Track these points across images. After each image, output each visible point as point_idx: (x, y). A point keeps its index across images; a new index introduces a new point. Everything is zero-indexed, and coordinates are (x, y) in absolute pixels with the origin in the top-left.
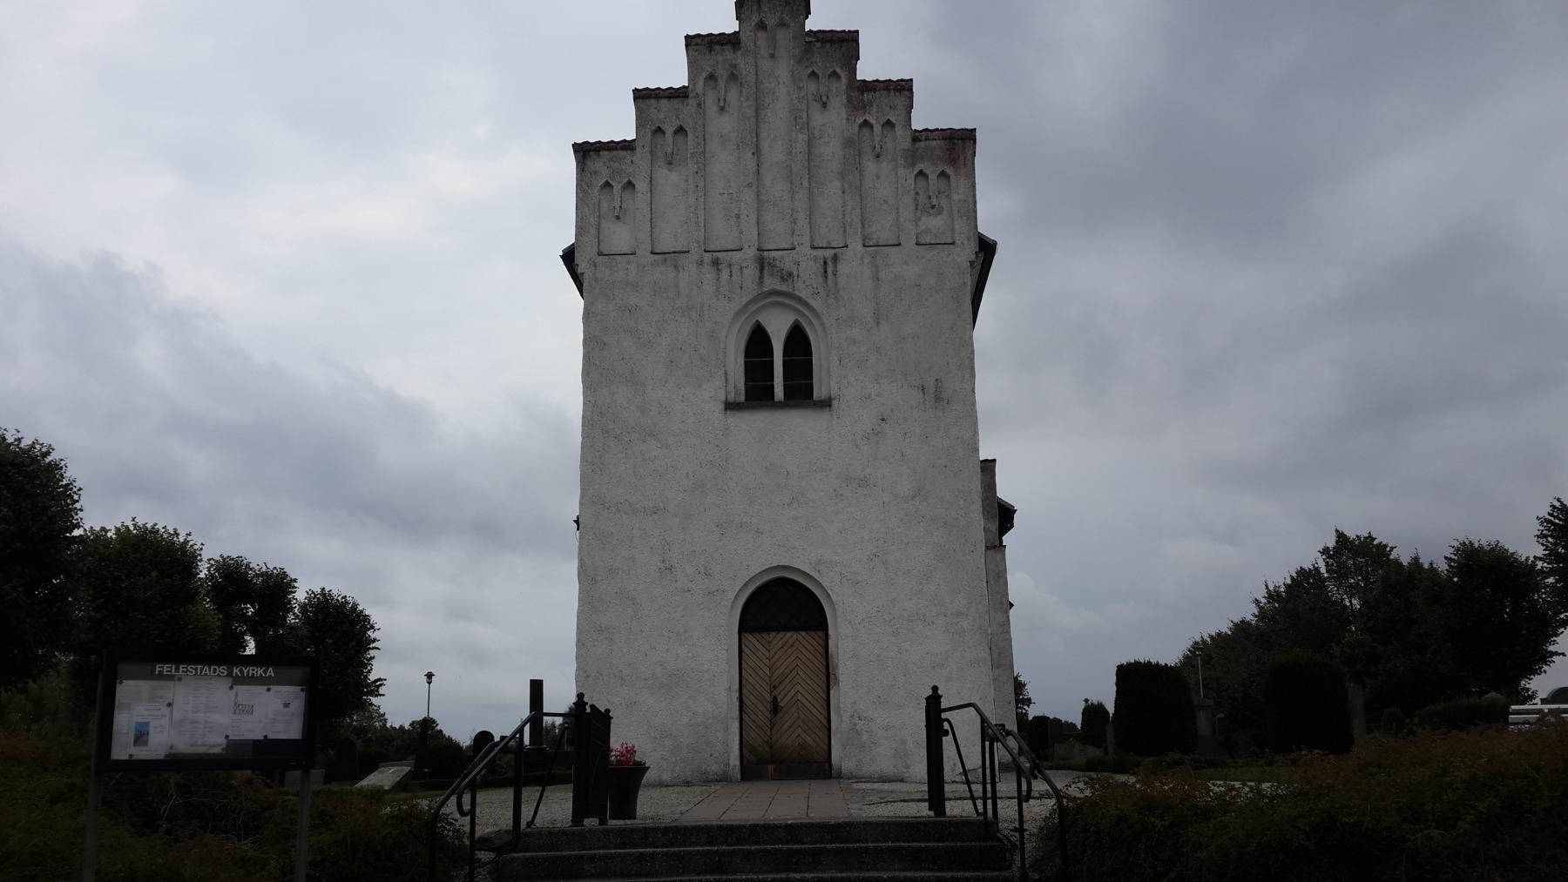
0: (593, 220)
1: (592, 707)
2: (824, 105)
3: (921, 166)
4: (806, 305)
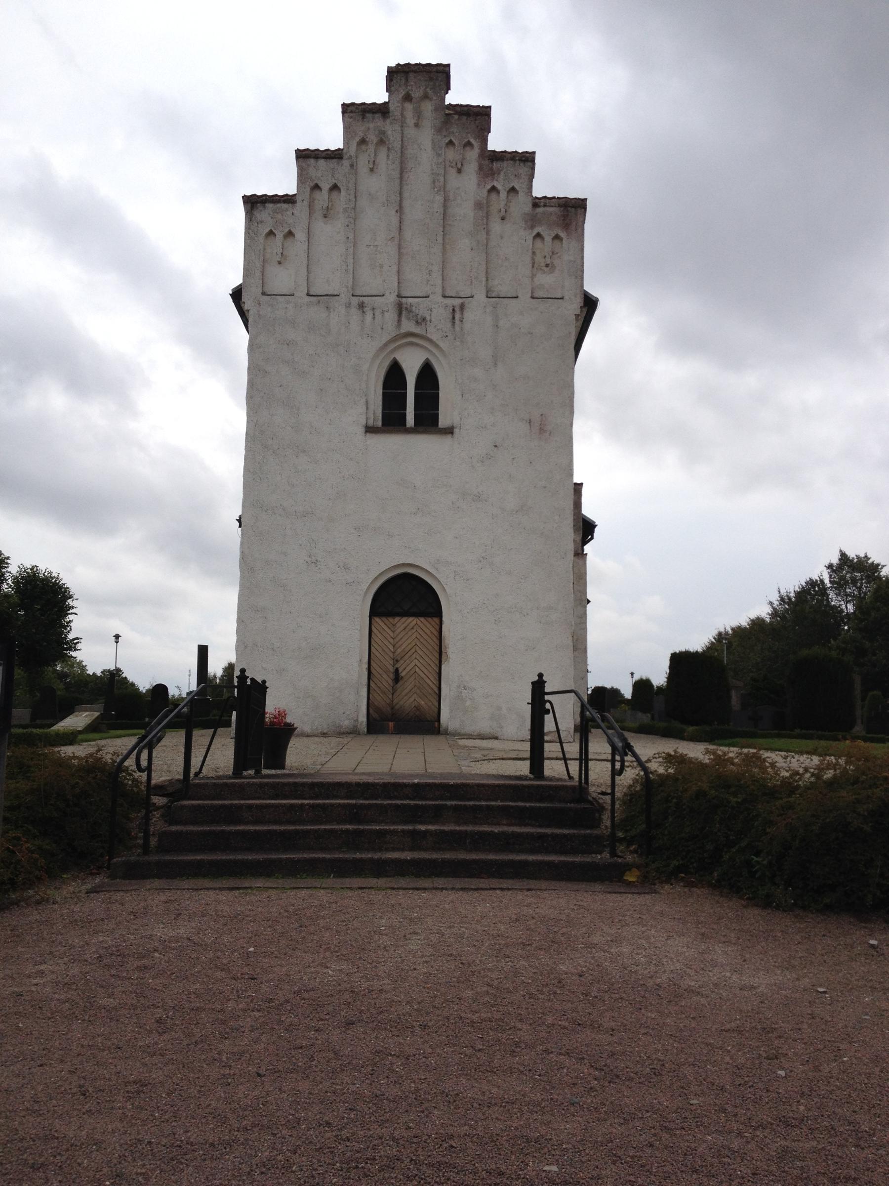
0: (258, 264)
1: (253, 680)
2: (459, 171)
4: (437, 346)
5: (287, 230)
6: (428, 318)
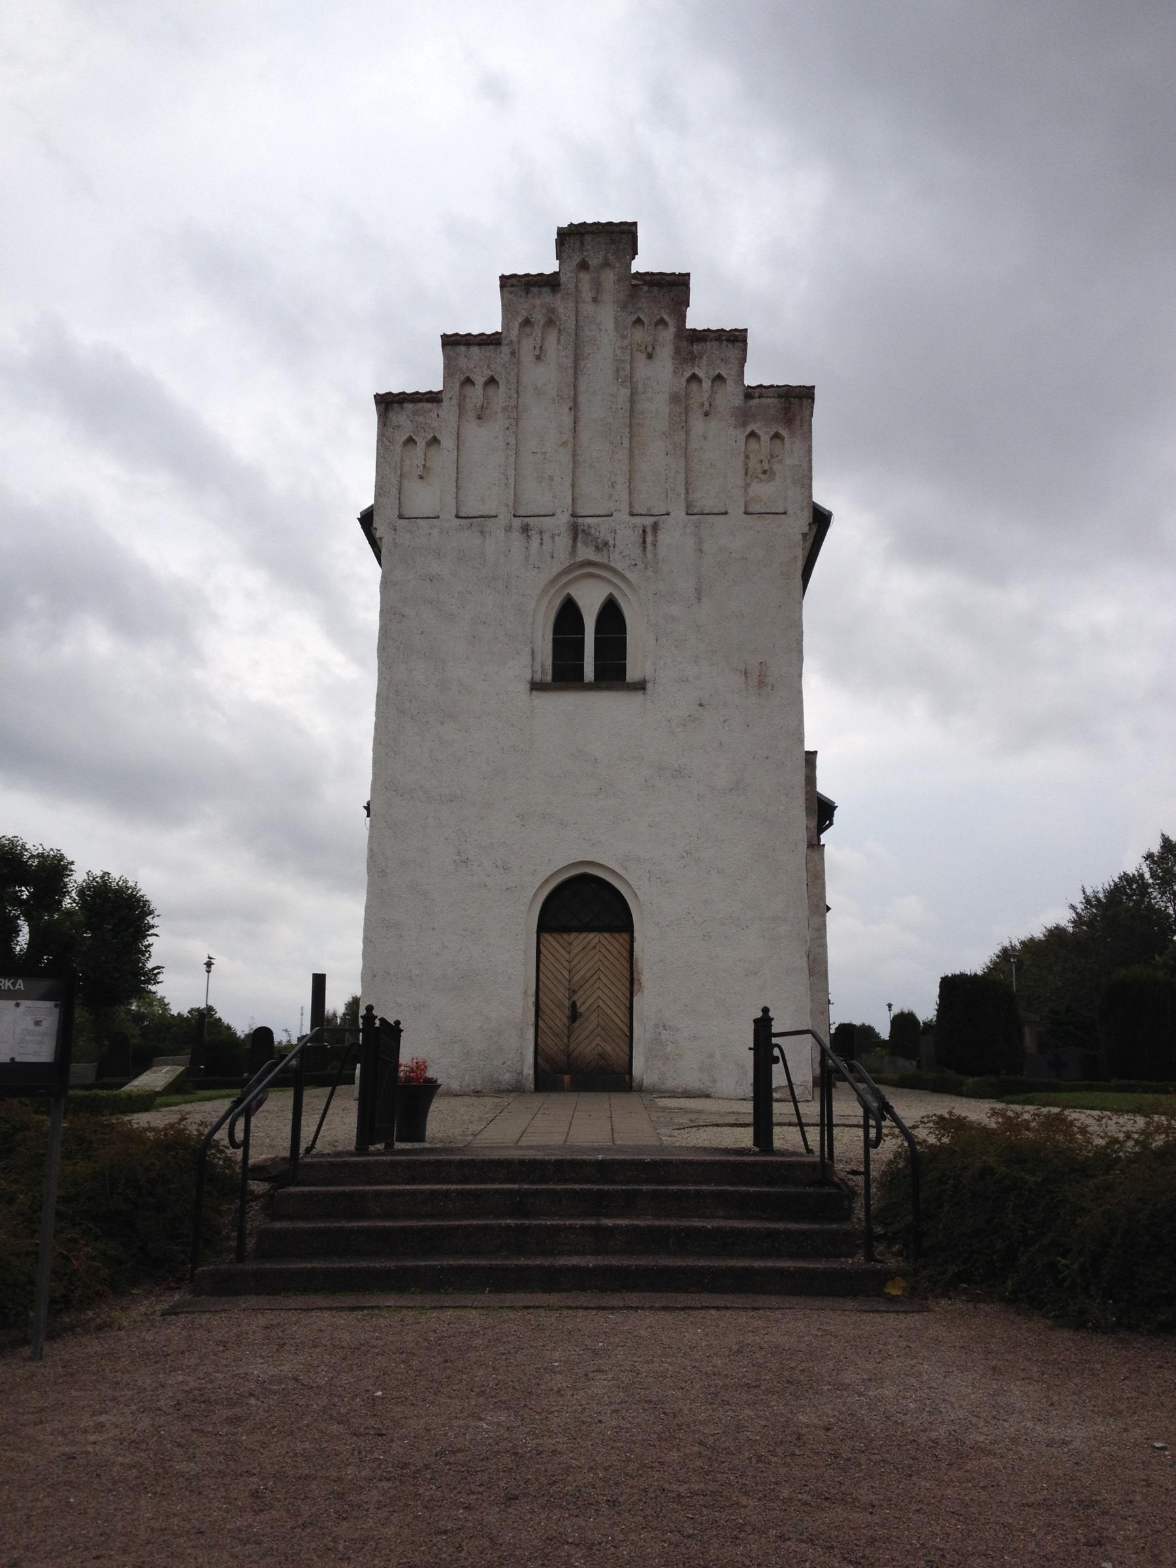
1: (382, 1020)
2: (650, 356)
3: (753, 427)
4: (623, 578)
5: (431, 436)
6: (611, 542)
